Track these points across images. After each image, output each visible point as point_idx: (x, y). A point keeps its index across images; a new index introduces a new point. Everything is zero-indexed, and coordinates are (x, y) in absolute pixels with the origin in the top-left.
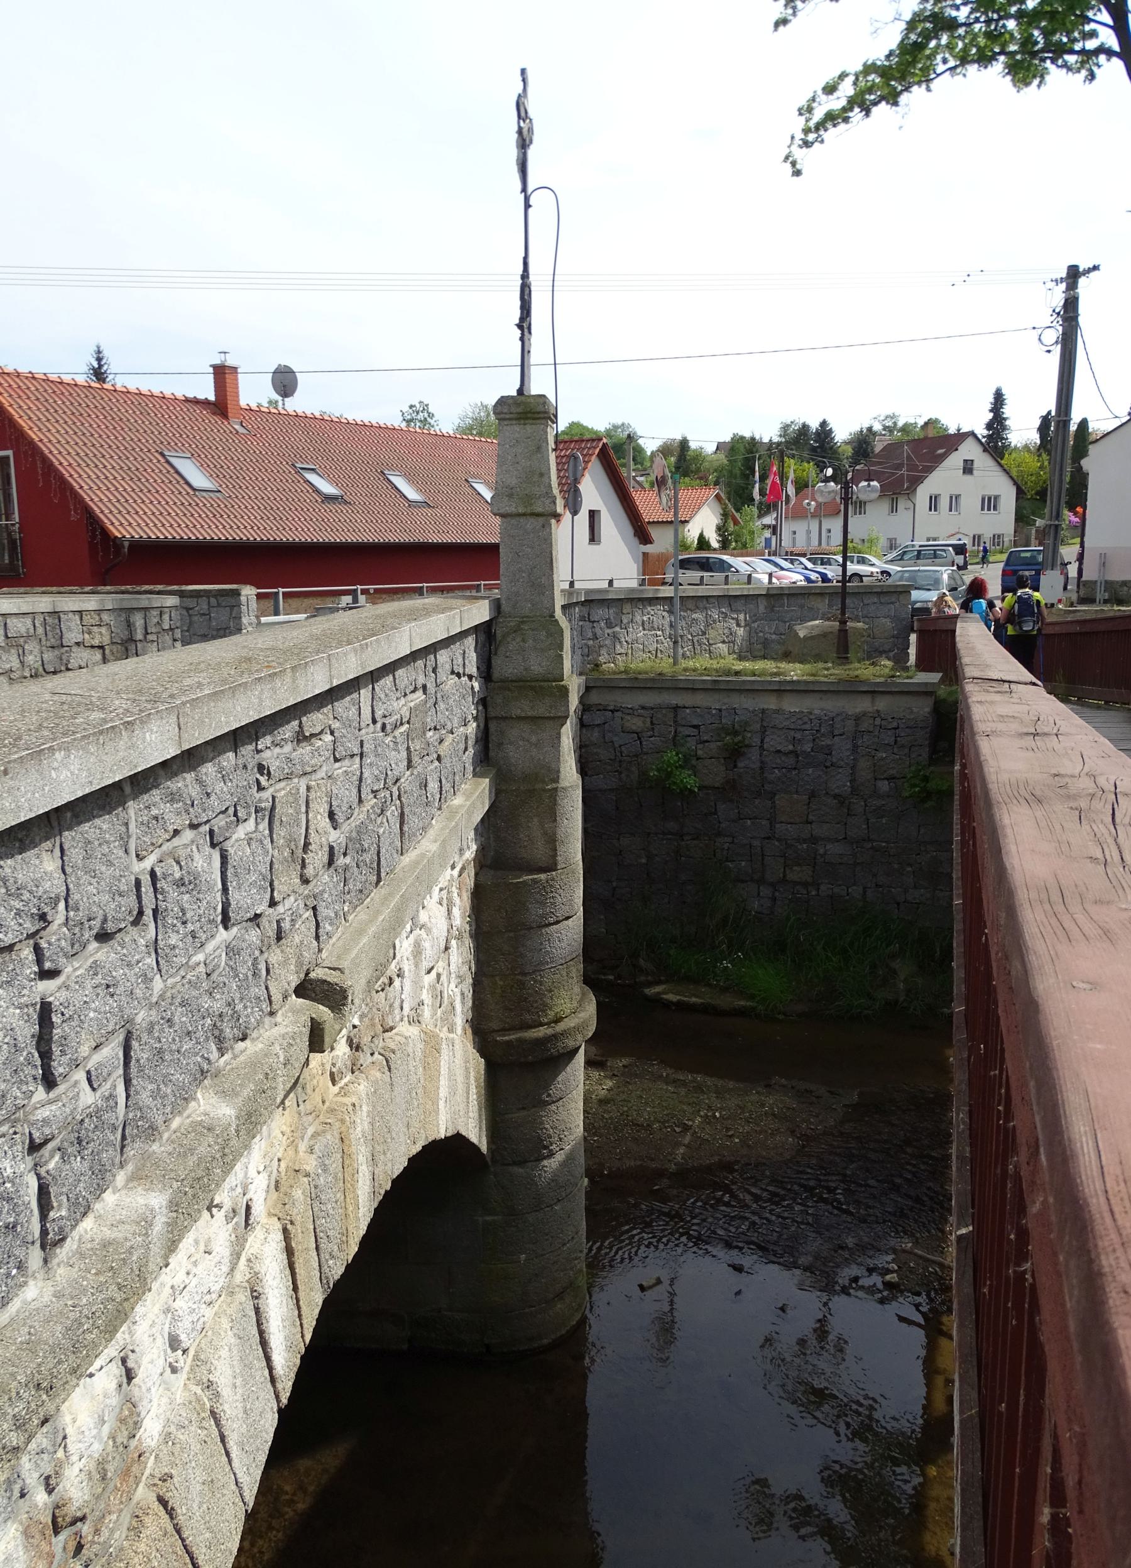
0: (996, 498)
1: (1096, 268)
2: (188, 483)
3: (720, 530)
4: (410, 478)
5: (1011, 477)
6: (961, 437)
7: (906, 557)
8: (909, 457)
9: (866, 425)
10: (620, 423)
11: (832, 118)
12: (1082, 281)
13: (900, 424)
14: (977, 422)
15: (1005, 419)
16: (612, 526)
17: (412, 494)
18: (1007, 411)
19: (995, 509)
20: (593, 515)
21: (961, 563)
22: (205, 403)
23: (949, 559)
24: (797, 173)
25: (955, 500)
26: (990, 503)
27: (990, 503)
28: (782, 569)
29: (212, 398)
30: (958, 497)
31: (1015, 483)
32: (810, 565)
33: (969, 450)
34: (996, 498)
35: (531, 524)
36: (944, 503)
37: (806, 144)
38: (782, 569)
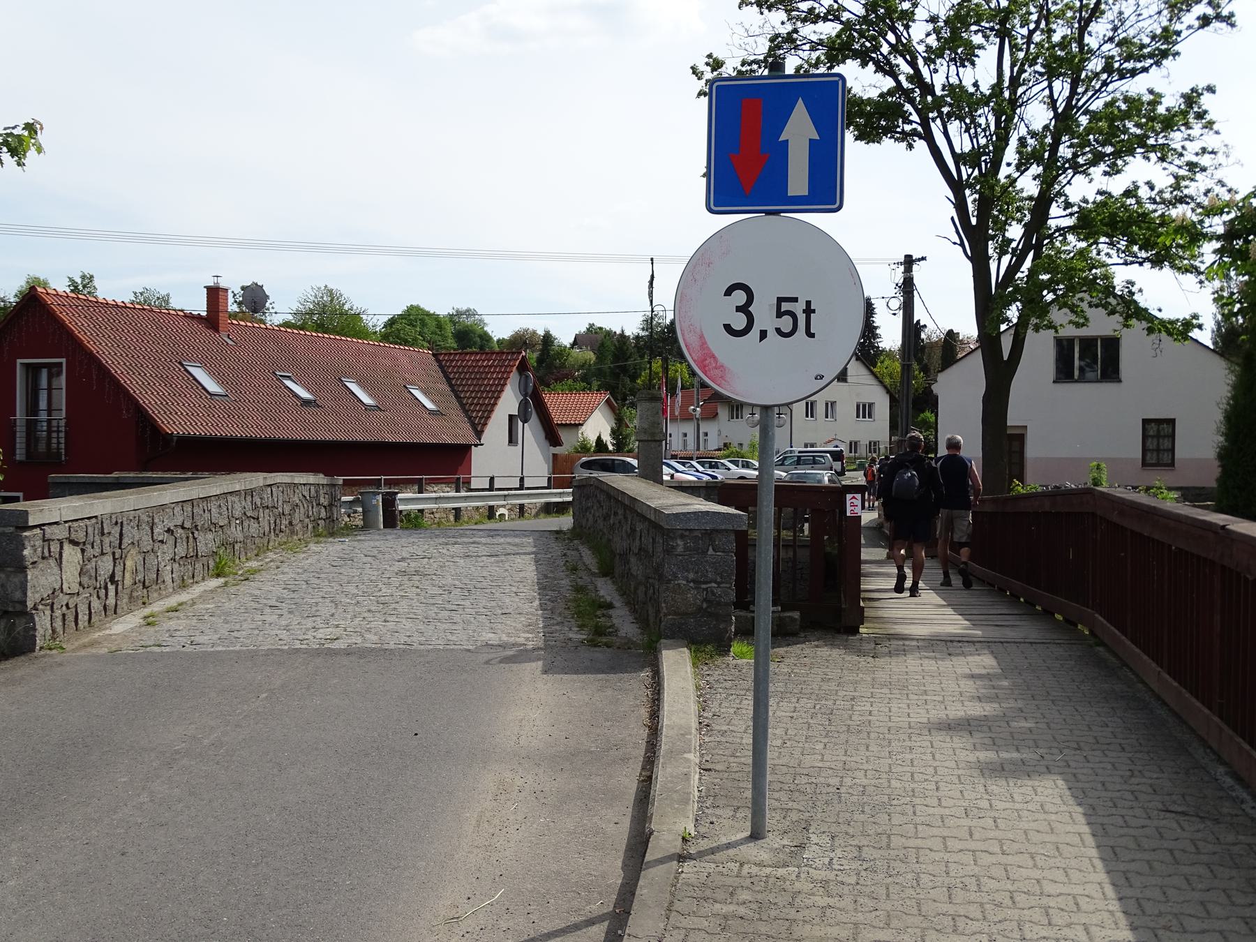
0: (871, 405)
1: (923, 259)
2: (204, 388)
3: (614, 433)
4: (426, 393)
5: (885, 387)
7: (787, 462)
10: (465, 308)
12: (915, 267)
15: (876, 328)
17: (367, 400)
19: (870, 416)
21: (839, 469)
22: (199, 317)
23: (828, 465)
25: (830, 406)
26: (865, 410)
27: (865, 410)
28: (677, 471)
29: (204, 314)
30: (833, 403)
31: (888, 392)
32: (700, 469)
34: (871, 405)
35: (653, 444)
36: (820, 409)
38: (677, 471)
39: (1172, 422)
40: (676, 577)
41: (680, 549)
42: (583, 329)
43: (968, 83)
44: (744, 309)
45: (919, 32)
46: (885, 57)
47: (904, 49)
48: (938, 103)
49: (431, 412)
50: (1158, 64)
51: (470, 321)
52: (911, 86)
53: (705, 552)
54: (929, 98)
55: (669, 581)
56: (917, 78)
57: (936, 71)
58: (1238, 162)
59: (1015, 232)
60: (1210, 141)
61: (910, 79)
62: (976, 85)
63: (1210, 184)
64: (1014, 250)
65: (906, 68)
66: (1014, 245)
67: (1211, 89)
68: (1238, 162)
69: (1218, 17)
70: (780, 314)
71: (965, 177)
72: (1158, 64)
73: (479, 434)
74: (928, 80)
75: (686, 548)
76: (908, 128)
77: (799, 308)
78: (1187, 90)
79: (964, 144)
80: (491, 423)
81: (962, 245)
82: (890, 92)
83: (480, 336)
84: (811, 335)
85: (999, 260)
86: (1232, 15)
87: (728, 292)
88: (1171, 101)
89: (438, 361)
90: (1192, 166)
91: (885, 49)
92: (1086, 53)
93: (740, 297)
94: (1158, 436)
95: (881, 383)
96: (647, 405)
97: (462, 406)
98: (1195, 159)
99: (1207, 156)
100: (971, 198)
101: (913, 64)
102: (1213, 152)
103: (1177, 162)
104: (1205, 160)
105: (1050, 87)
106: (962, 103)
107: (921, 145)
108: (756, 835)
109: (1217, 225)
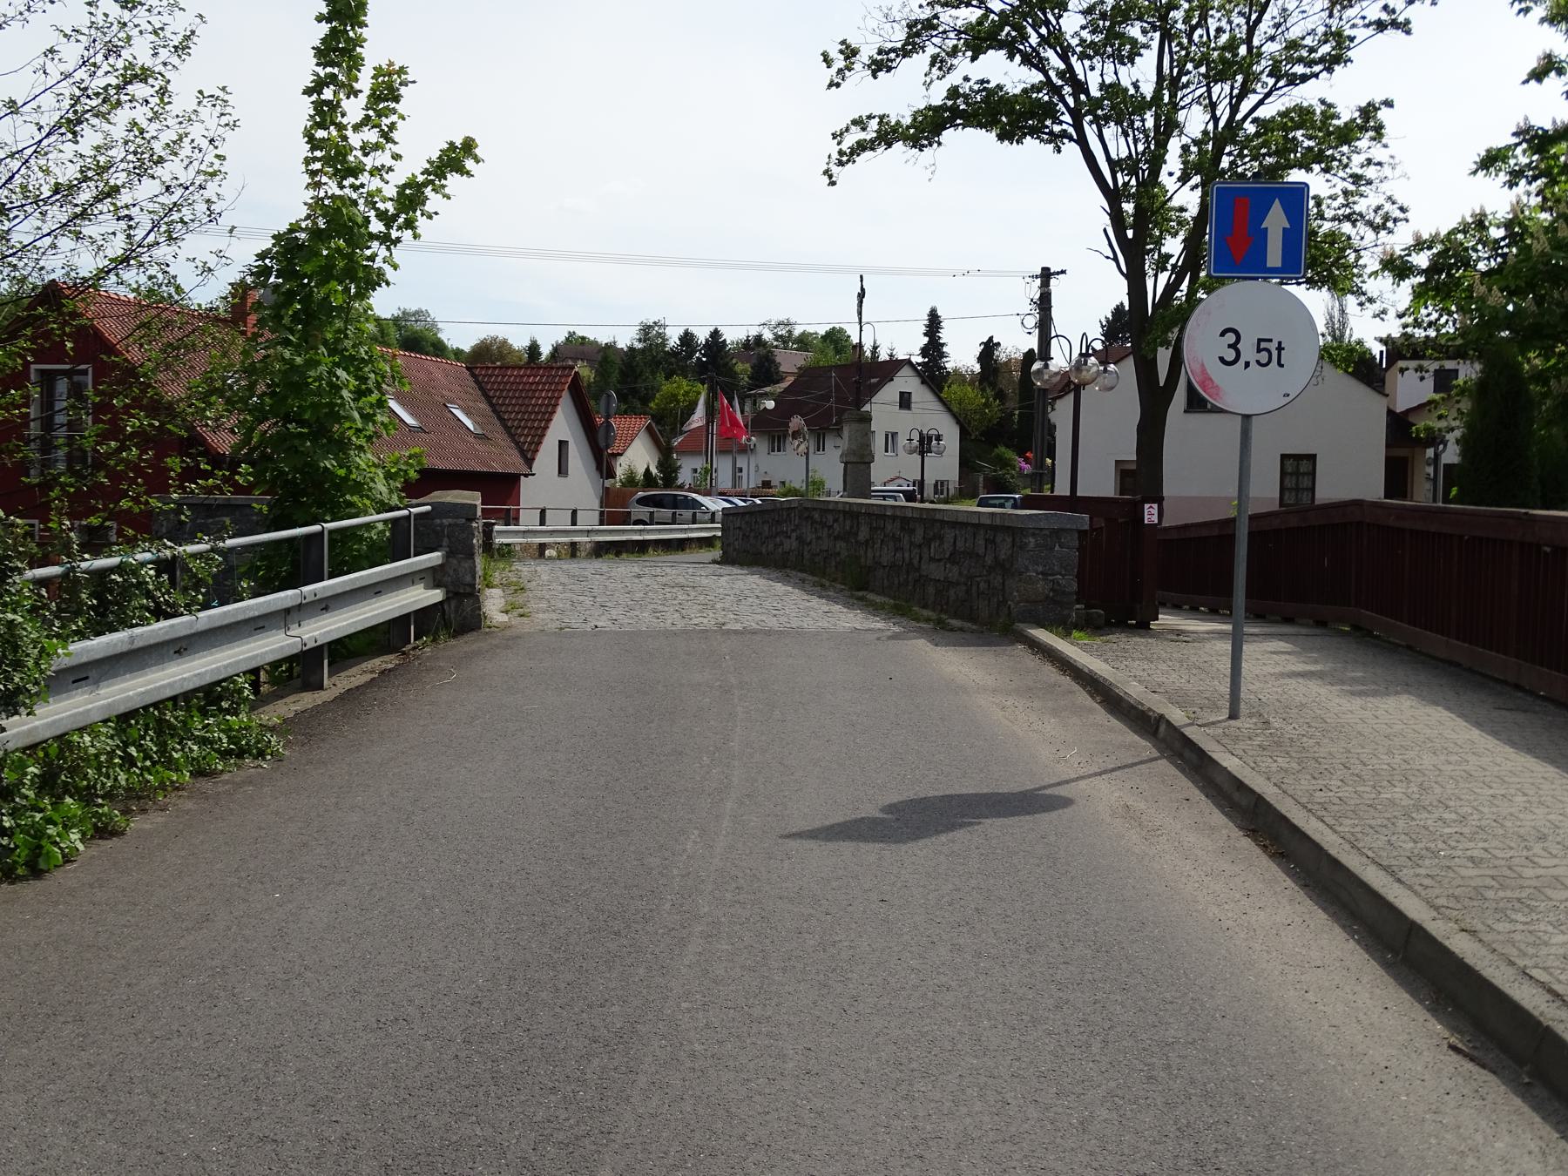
1: (1063, 272)
3: (660, 466)
4: (468, 414)
6: (895, 366)
8: (837, 384)
9: (753, 332)
10: (414, 309)
11: (861, 147)
12: (1053, 281)
13: (797, 332)
14: (907, 343)
16: (579, 459)
17: (410, 420)
18: (945, 335)
20: (563, 445)
24: (833, 183)
30: (894, 435)
31: (958, 422)
33: (906, 382)
37: (841, 164)
39: (1312, 458)
40: (1027, 569)
41: (1032, 545)
42: (561, 339)
43: (1126, 82)
44: (1233, 346)
45: (1071, 24)
46: (1034, 49)
47: (1055, 39)
48: (1096, 104)
49: (476, 436)
50: (1330, 70)
51: (418, 326)
52: (1060, 83)
53: (1052, 549)
54: (1083, 97)
55: (1021, 573)
56: (1069, 75)
57: (1092, 68)
58: (1405, 175)
59: (1173, 246)
60: (1378, 153)
61: (1060, 74)
62: (1136, 85)
63: (1380, 200)
64: (1174, 266)
65: (1055, 62)
66: (1173, 261)
67: (1389, 104)
68: (1405, 175)
69: (1395, 24)
70: (1259, 350)
71: (1120, 183)
72: (1330, 70)
73: (529, 462)
74: (1081, 77)
75: (1037, 545)
76: (1057, 128)
77: (1273, 346)
78: (1363, 104)
79: (1119, 149)
80: (543, 448)
81: (1116, 259)
82: (1036, 88)
83: (433, 345)
84: (1281, 365)
85: (1156, 276)
86: (1408, 22)
87: (1223, 334)
88: (1346, 113)
89: (473, 375)
90: (1357, 179)
91: (1034, 39)
92: (1255, 54)
93: (1231, 338)
94: (1297, 473)
95: (949, 410)
96: (855, 426)
97: (507, 429)
98: (1359, 171)
99: (1372, 168)
100: (1128, 207)
101: (1064, 57)
102: (1380, 164)
103: (1341, 174)
104: (1371, 172)
105: (1209, 91)
106: (1120, 105)
107: (1071, 150)
108: (1233, 715)
109: (1422, 260)
